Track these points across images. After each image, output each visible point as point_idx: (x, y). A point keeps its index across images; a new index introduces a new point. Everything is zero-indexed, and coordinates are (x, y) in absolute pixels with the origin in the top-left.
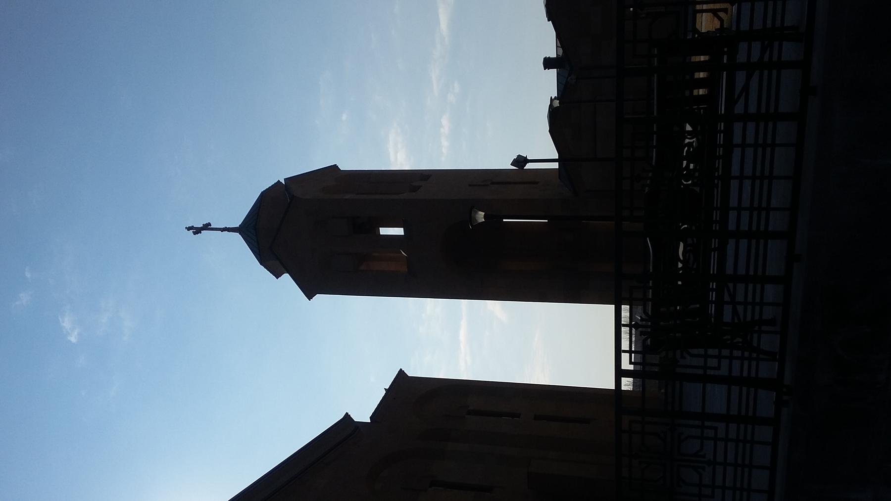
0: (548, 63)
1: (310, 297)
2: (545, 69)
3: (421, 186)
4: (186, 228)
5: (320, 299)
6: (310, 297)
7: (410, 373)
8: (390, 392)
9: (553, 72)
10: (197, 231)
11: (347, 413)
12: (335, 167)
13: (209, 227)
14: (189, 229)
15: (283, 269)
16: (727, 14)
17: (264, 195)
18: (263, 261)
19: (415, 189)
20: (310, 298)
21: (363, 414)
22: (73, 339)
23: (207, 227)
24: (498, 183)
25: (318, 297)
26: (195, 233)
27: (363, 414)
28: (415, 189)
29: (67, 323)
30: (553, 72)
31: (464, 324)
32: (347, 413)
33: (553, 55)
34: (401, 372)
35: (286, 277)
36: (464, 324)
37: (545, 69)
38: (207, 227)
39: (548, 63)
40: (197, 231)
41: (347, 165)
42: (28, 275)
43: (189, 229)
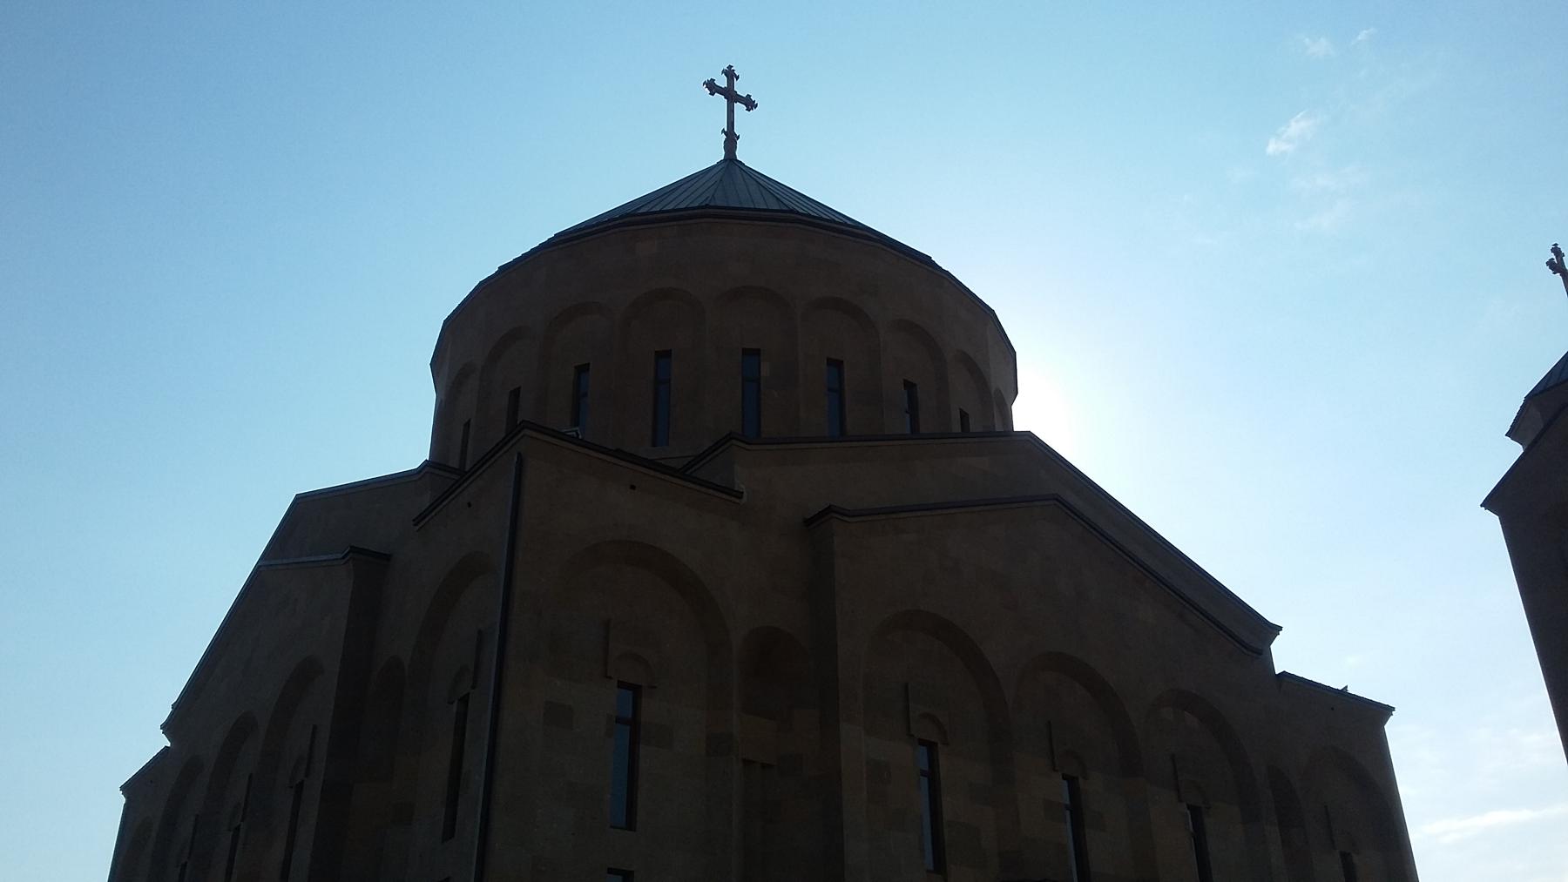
2: (1481, 506)
3: (519, 388)
4: (1556, 245)
5: (1492, 523)
7: (1391, 728)
8: (1342, 697)
11: (1280, 628)
13: (1555, 260)
14: (1556, 250)
15: (1531, 438)
20: (1489, 503)
21: (1286, 657)
22: (1272, 147)
25: (1493, 521)
26: (1550, 264)
27: (1286, 657)
29: (1298, 127)
31: (1524, 815)
32: (1280, 628)
35: (1516, 450)
36: (1524, 815)
37: (1481, 506)
42: (1362, 36)
43: (1556, 250)
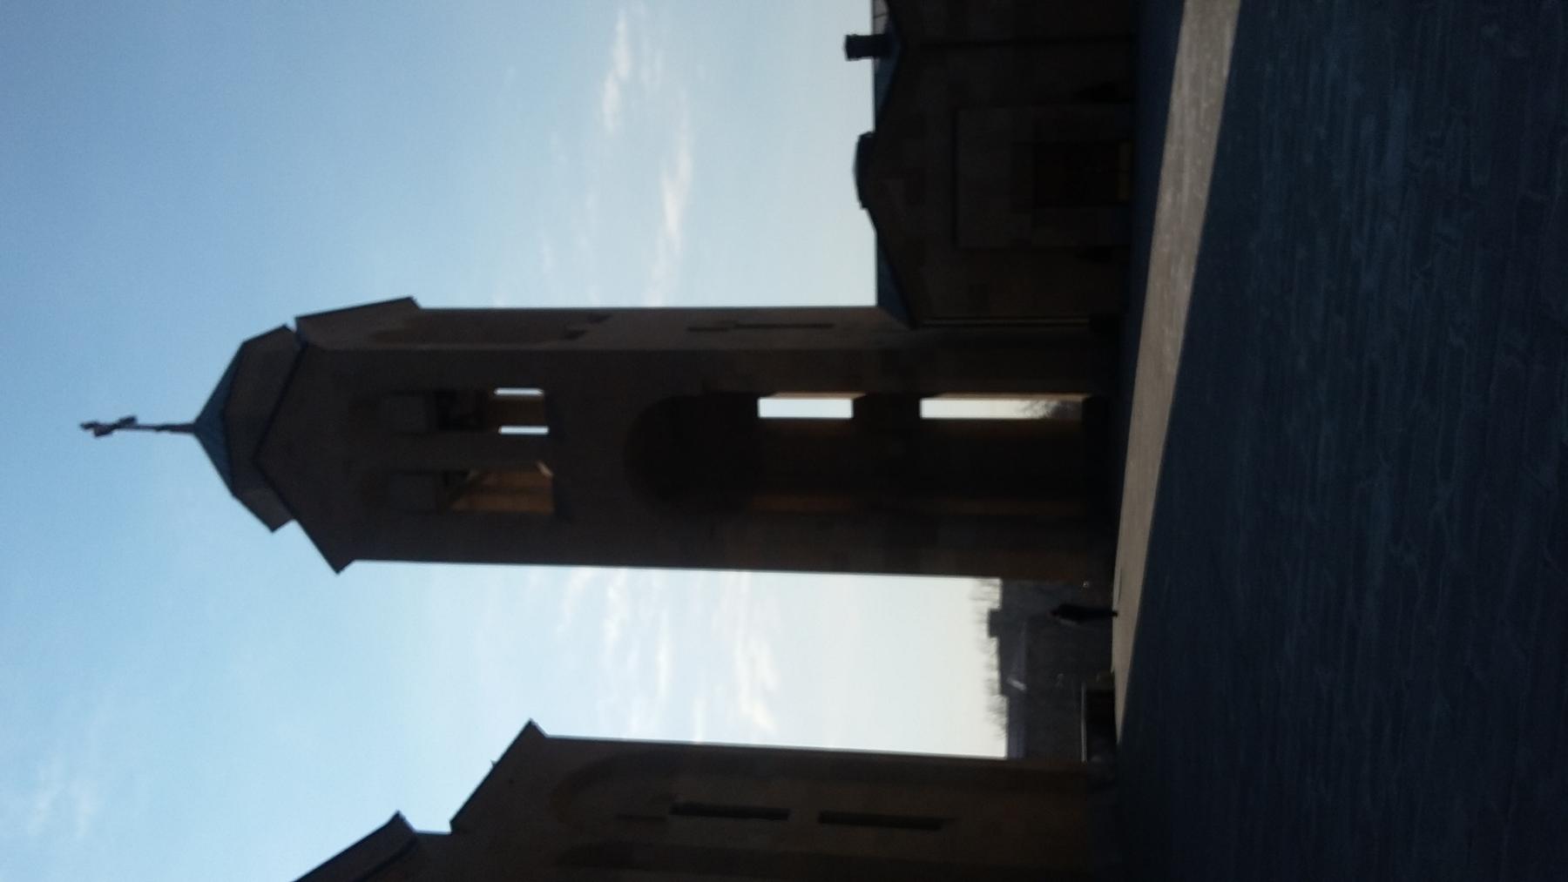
0: (856, 47)
1: (338, 564)
6: (338, 564)
7: (552, 728)
9: (865, 67)
10: (101, 430)
12: (408, 303)
14: (87, 426)
16: (1055, 613)
17: (249, 350)
18: (238, 487)
19: (573, 335)
23: (128, 423)
24: (750, 327)
28: (573, 335)
30: (865, 67)
33: (864, 28)
34: (531, 731)
35: (293, 531)
38: (128, 423)
39: (856, 47)
40: (101, 430)
41: (429, 299)
43: (87, 426)
